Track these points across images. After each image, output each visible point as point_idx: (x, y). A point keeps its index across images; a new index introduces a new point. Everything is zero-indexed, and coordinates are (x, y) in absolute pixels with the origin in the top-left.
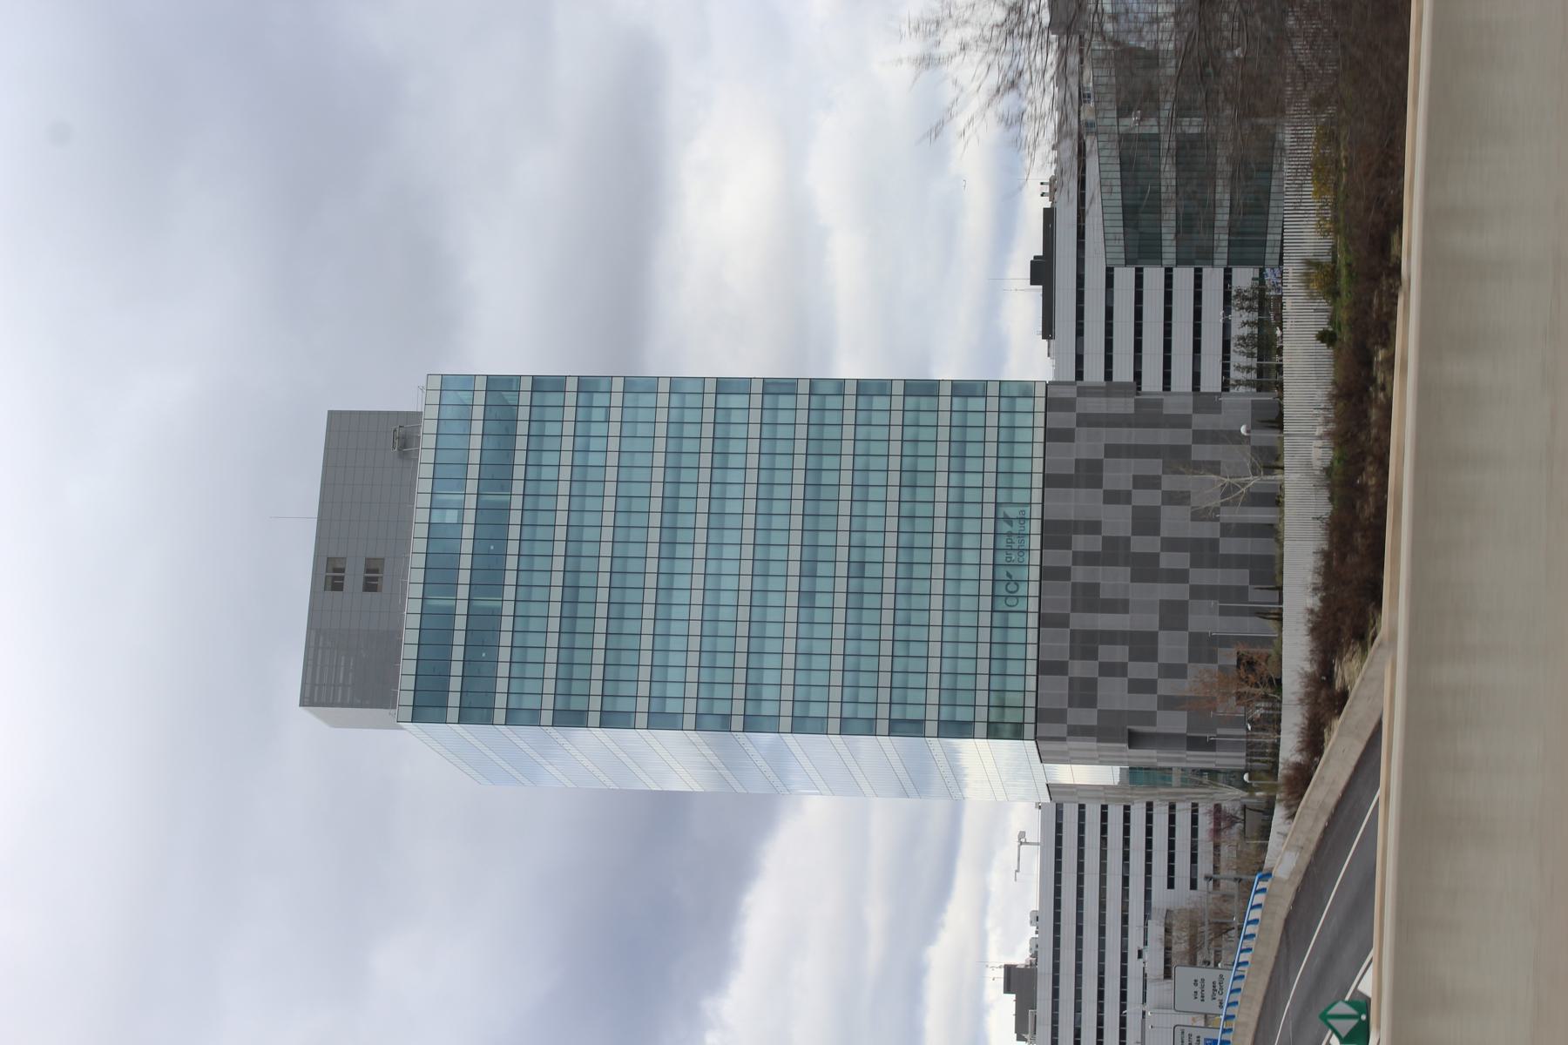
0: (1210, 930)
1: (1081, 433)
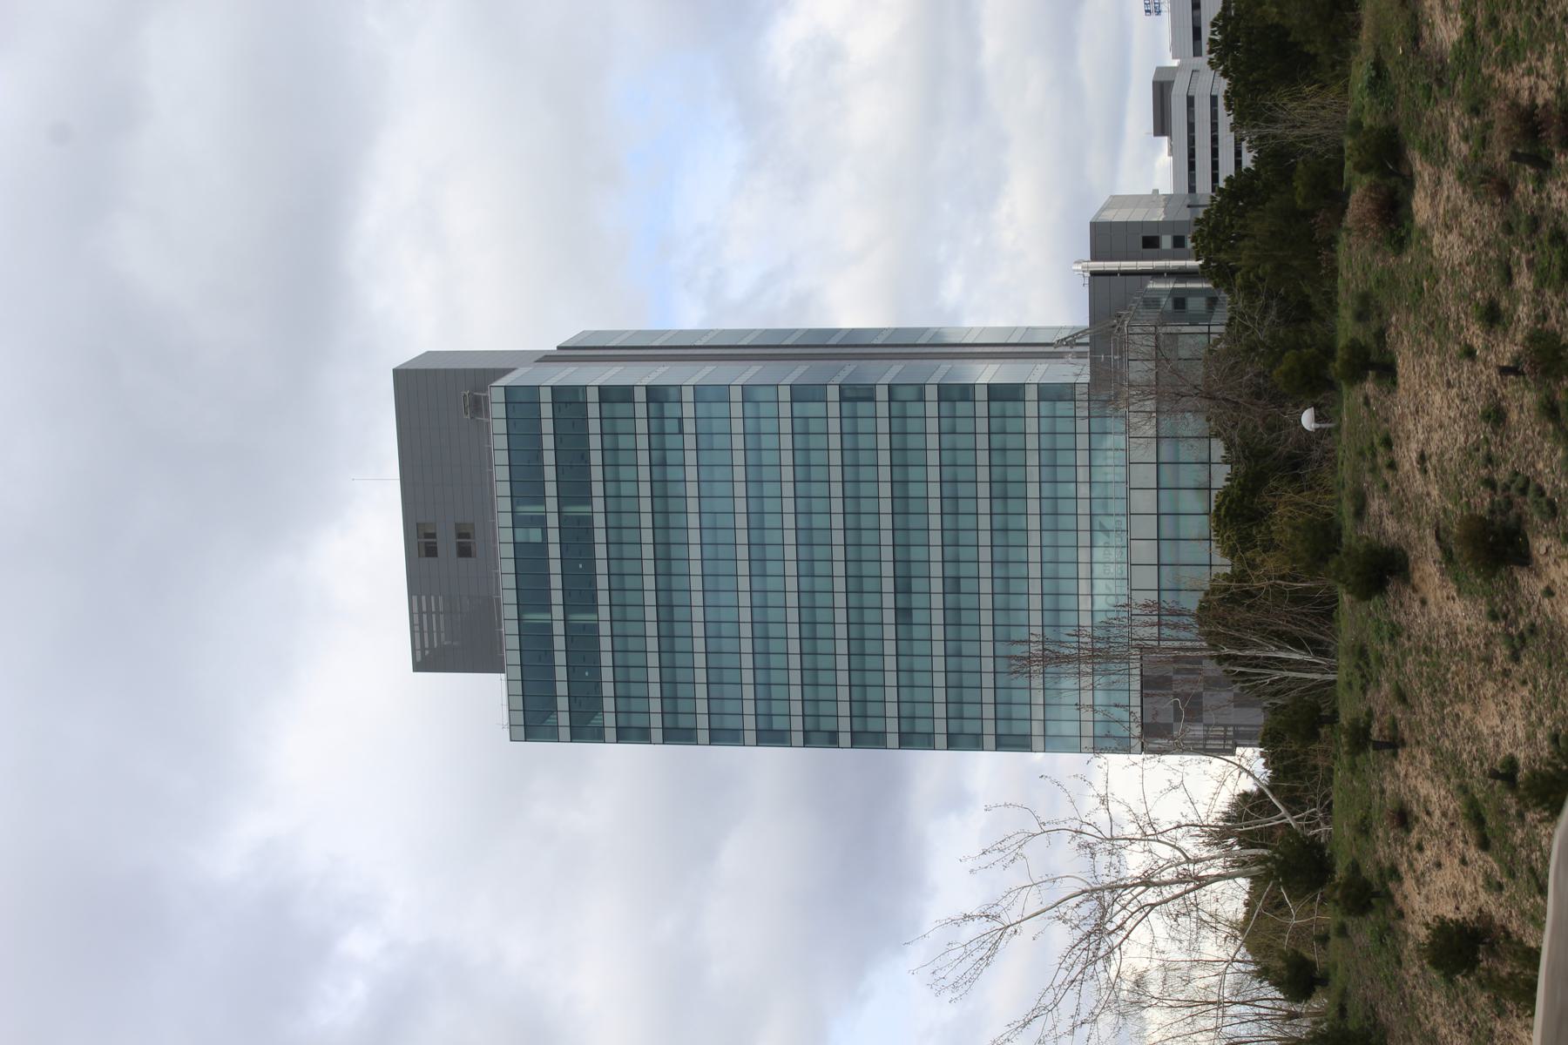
0: (1376, 249)
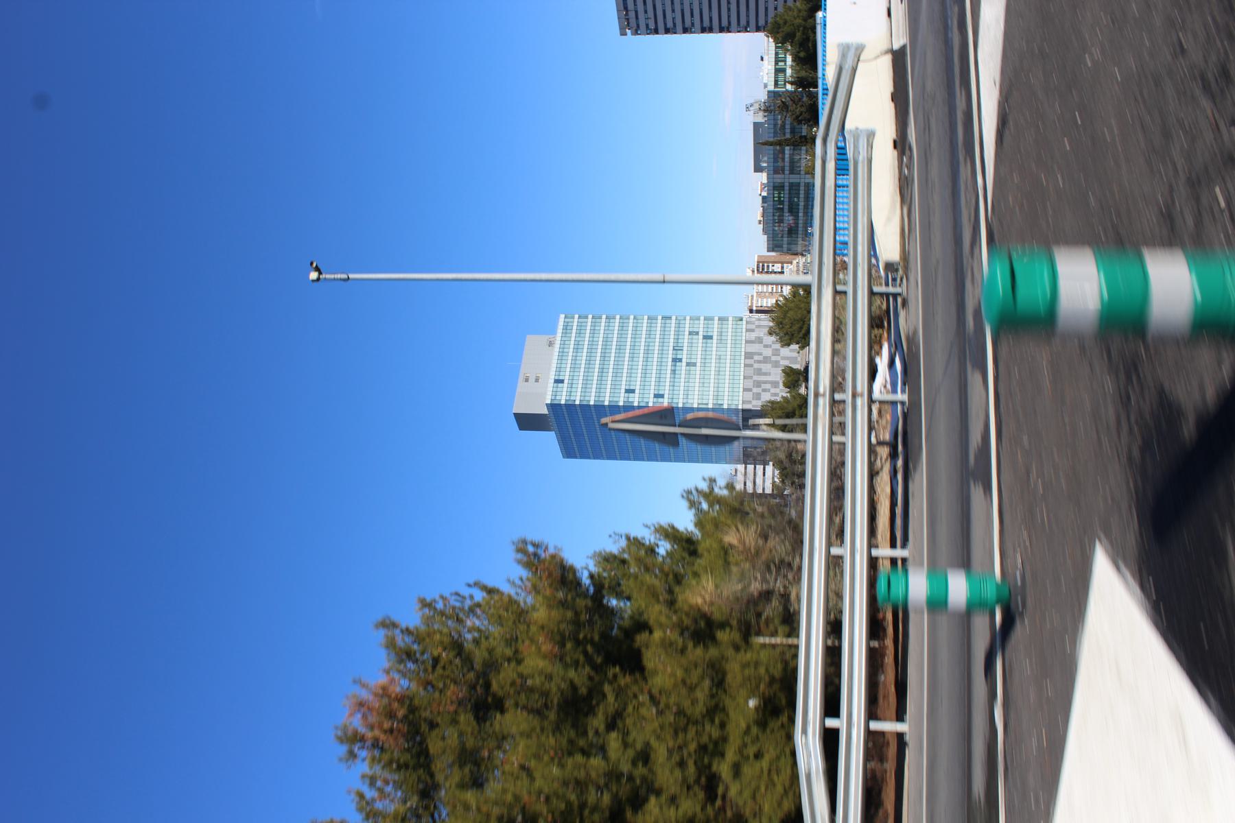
1: (757, 330)
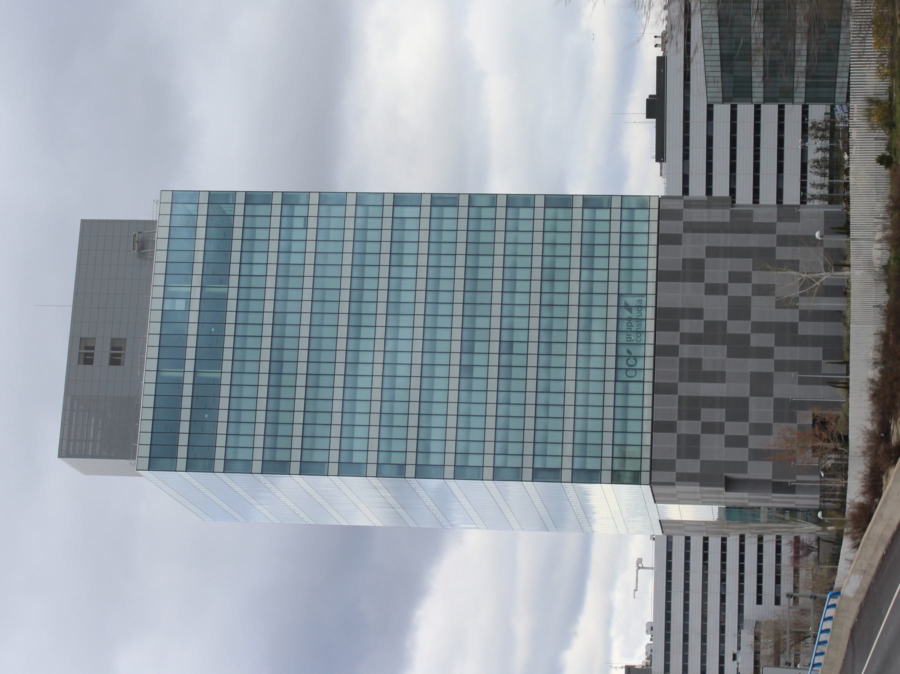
1: (688, 237)
